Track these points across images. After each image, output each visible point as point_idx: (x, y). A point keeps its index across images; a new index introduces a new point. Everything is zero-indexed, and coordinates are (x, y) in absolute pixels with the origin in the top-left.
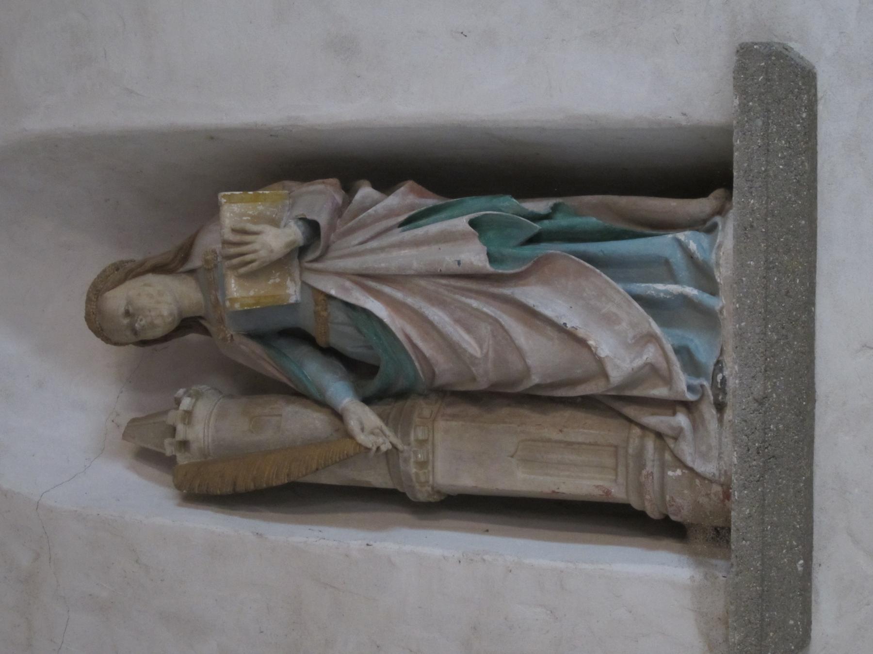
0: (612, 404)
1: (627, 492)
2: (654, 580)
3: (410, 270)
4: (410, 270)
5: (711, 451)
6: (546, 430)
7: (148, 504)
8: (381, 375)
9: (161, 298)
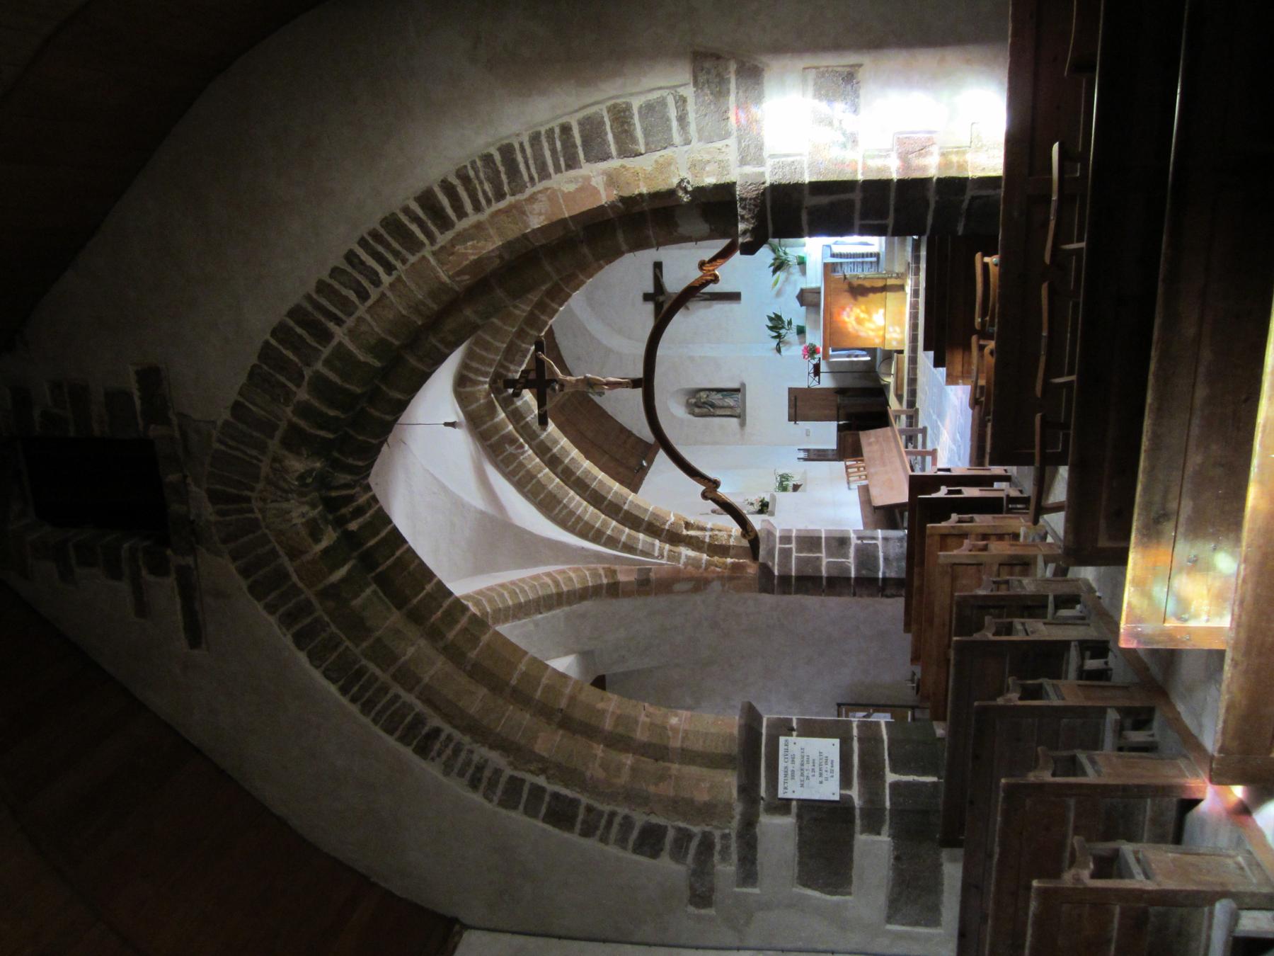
0: (731, 407)
1: (845, 781)
2: (735, 420)
3: (715, 398)
4: (715, 398)
5: (738, 411)
6: (551, 487)
7: (691, 417)
8: (713, 405)
9: (693, 401)
